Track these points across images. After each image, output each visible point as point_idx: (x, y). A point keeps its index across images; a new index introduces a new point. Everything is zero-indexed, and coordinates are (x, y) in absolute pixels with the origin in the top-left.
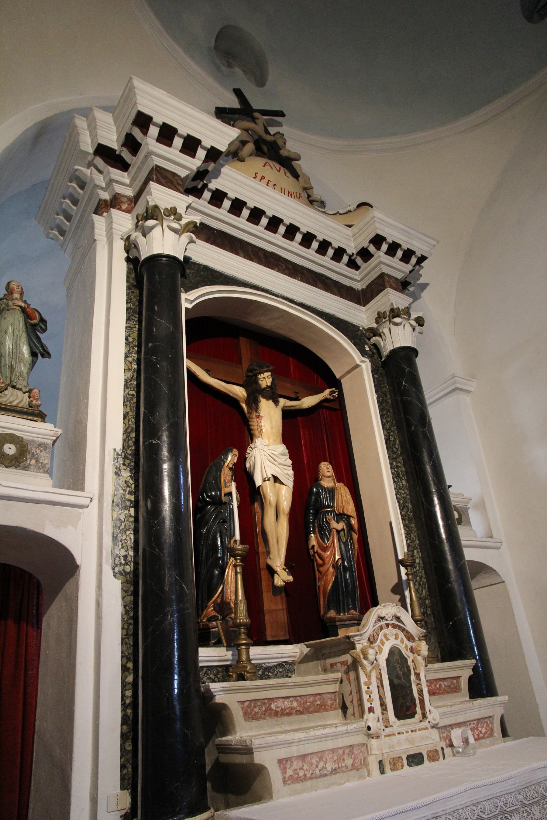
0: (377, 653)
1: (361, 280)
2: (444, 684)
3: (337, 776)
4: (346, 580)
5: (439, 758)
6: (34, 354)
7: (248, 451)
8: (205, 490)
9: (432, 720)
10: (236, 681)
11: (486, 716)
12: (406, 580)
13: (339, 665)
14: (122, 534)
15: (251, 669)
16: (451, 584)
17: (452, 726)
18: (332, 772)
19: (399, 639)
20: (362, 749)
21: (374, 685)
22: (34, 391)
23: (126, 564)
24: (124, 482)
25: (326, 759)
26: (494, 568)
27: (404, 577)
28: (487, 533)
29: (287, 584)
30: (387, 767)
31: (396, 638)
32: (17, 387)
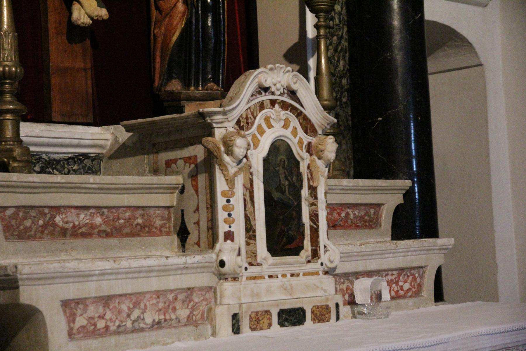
0: (249, 145)
3: (161, 332)
11: (415, 265)
13: (180, 163)
15: (21, 155)
16: (392, 52)
17: (357, 275)
18: (153, 326)
19: (290, 129)
20: (208, 296)
21: (239, 199)
25: (145, 305)
27: (311, 33)
29: (96, 22)
30: (245, 324)
31: (286, 126)
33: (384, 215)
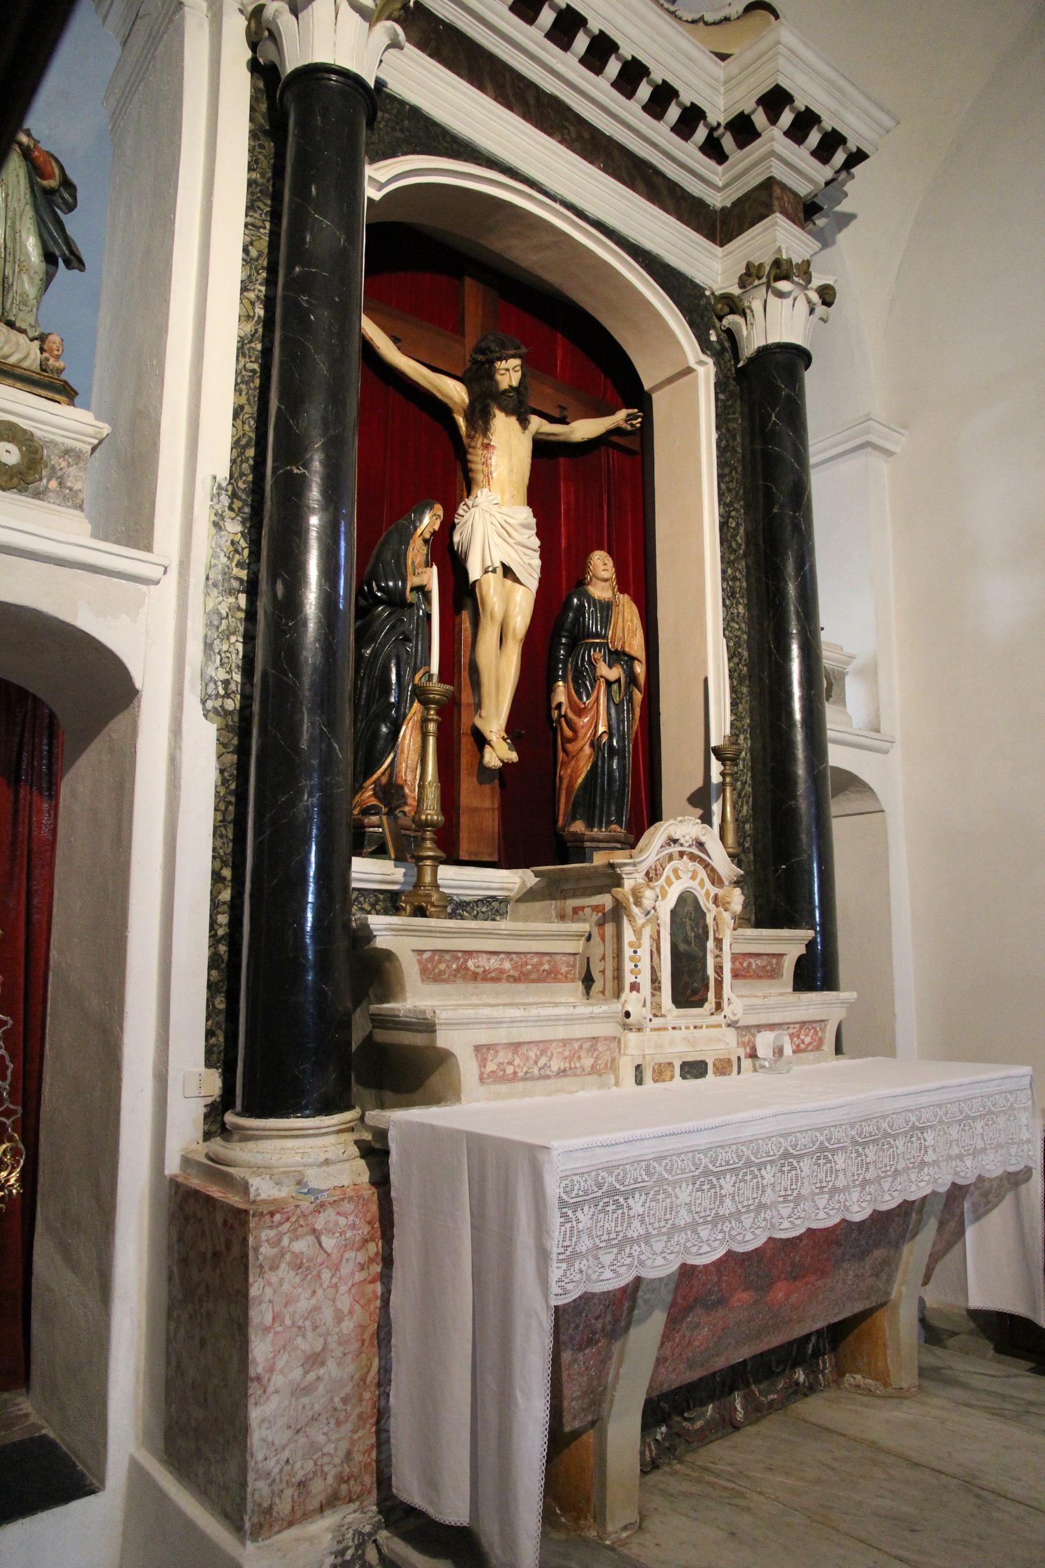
1: (726, 186)
2: (755, 963)
3: (566, 1080)
4: (611, 771)
5: (731, 1071)
6: (50, 258)
7: (460, 511)
8: (374, 576)
9: (729, 1015)
10: (410, 915)
12: (717, 785)
13: (588, 910)
14: (222, 640)
15: (439, 900)
16: (797, 801)
17: (759, 1028)
19: (698, 880)
21: (646, 948)
22: (51, 338)
23: (227, 695)
24: (229, 543)
26: (867, 781)
27: (716, 778)
28: (876, 721)
29: (506, 765)
30: (648, 1075)
31: (693, 878)
32: (18, 324)
33: (786, 965)
